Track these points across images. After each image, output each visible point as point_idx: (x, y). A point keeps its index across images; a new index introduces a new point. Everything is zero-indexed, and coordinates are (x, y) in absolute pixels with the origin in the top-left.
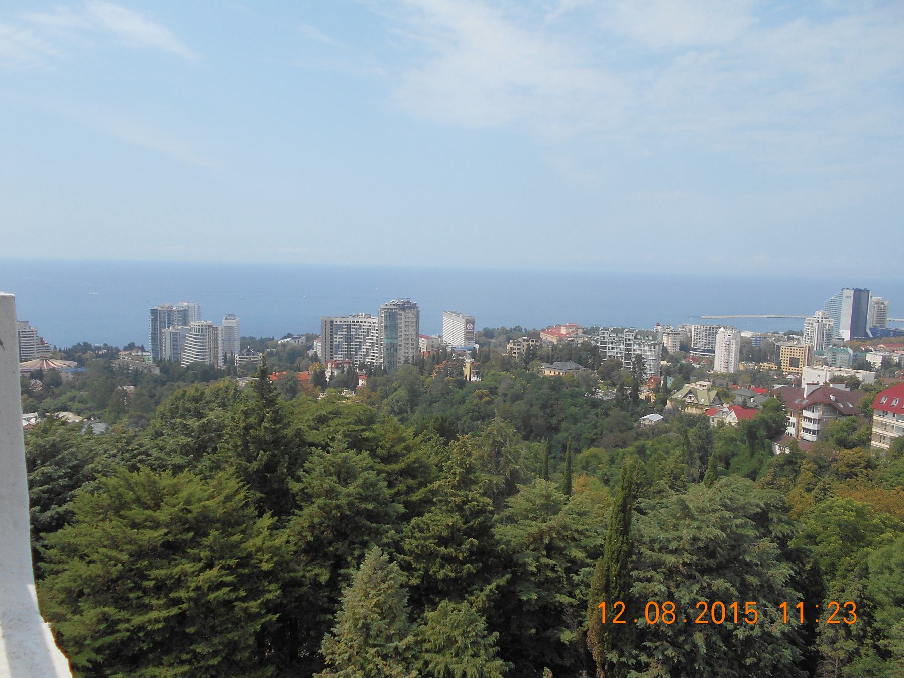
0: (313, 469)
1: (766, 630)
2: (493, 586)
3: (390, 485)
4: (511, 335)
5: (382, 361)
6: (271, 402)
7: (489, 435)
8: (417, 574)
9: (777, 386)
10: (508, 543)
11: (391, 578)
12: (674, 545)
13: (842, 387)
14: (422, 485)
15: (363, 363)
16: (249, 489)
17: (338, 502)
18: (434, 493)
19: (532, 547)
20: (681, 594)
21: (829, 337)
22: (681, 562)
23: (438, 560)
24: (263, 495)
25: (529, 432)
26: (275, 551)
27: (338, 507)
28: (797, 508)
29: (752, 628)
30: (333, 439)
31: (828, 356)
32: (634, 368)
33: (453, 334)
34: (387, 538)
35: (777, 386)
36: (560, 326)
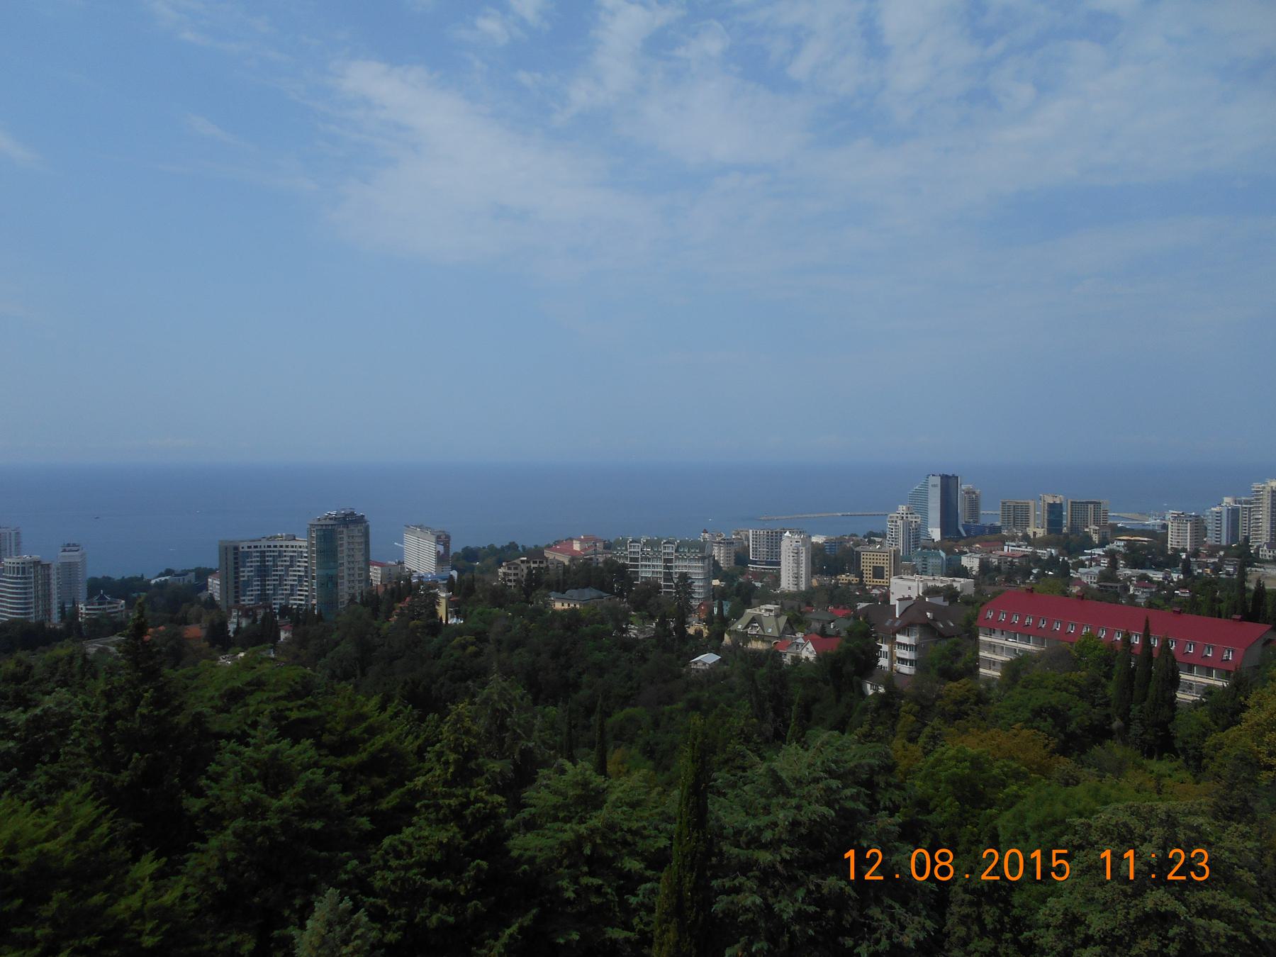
0: (223, 774)
1: (896, 940)
2: (514, 929)
3: (346, 790)
4: (507, 553)
5: (314, 602)
6: (151, 674)
7: (485, 702)
8: (395, 925)
9: (862, 605)
10: (531, 861)
11: (357, 937)
12: (768, 836)
13: (939, 601)
14: (393, 785)
15: (286, 606)
16: (116, 816)
17: (266, 823)
18: (416, 795)
19: (566, 862)
20: (782, 906)
21: (917, 538)
22: (779, 859)
23: (428, 900)
24: (140, 825)
25: (540, 691)
26: (164, 914)
27: (266, 831)
28: (903, 764)
29: (878, 942)
30: (254, 725)
31: (917, 561)
32: (677, 592)
33: (420, 558)
34: (346, 872)
35: (862, 605)
36: (571, 539)
